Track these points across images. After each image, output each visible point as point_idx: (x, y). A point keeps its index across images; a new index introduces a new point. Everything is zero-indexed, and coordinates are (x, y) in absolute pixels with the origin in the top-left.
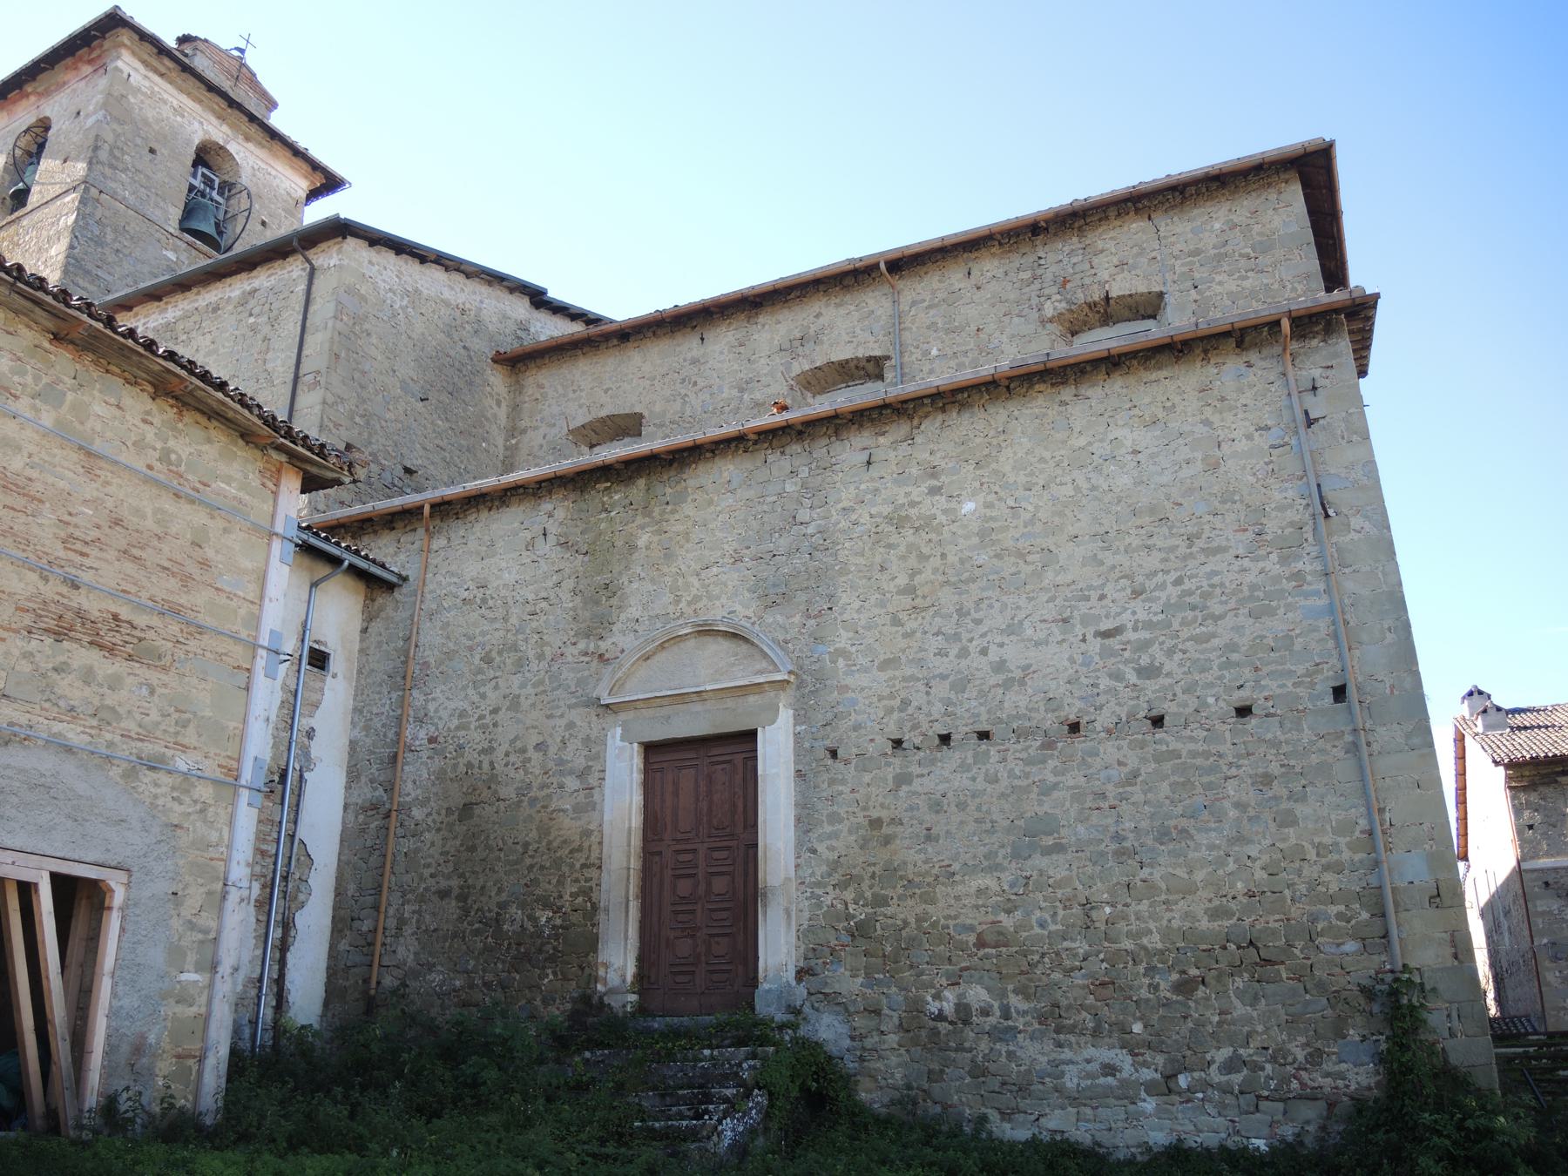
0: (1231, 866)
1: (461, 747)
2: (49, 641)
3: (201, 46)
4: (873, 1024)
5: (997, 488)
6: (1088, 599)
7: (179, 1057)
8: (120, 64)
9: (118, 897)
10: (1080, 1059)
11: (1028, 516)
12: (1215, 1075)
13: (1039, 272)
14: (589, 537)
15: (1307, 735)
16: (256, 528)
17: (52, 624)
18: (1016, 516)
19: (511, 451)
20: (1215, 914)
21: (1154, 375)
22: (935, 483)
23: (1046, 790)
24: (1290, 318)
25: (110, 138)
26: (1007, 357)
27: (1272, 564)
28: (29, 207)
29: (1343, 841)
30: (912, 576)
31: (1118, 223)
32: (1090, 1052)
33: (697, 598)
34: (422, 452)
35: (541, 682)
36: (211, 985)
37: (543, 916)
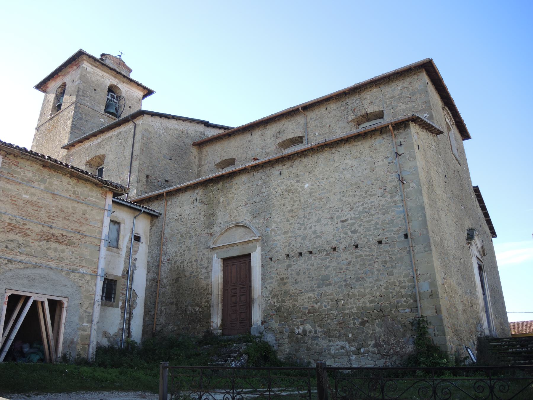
0: (376, 288)
1: (176, 262)
2: (45, 242)
3: (108, 56)
4: (281, 336)
5: (314, 180)
6: (338, 211)
7: (83, 345)
8: (84, 65)
9: (66, 305)
10: (335, 345)
11: (323, 187)
12: (371, 349)
13: (347, 107)
14: (208, 199)
15: (397, 249)
16: (100, 208)
17: (46, 238)
18: (319, 188)
19: (199, 171)
20: (371, 302)
21: (357, 144)
22: (298, 179)
23: (327, 268)
24: (392, 125)
25: (82, 88)
26: (340, 134)
27: (388, 199)
28: (61, 110)
29: (406, 279)
30: (292, 207)
31: (370, 89)
32: (338, 343)
33: (236, 216)
34: (171, 175)
35: (196, 242)
36: (91, 327)
37: (197, 309)
